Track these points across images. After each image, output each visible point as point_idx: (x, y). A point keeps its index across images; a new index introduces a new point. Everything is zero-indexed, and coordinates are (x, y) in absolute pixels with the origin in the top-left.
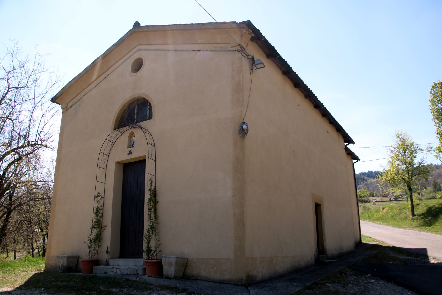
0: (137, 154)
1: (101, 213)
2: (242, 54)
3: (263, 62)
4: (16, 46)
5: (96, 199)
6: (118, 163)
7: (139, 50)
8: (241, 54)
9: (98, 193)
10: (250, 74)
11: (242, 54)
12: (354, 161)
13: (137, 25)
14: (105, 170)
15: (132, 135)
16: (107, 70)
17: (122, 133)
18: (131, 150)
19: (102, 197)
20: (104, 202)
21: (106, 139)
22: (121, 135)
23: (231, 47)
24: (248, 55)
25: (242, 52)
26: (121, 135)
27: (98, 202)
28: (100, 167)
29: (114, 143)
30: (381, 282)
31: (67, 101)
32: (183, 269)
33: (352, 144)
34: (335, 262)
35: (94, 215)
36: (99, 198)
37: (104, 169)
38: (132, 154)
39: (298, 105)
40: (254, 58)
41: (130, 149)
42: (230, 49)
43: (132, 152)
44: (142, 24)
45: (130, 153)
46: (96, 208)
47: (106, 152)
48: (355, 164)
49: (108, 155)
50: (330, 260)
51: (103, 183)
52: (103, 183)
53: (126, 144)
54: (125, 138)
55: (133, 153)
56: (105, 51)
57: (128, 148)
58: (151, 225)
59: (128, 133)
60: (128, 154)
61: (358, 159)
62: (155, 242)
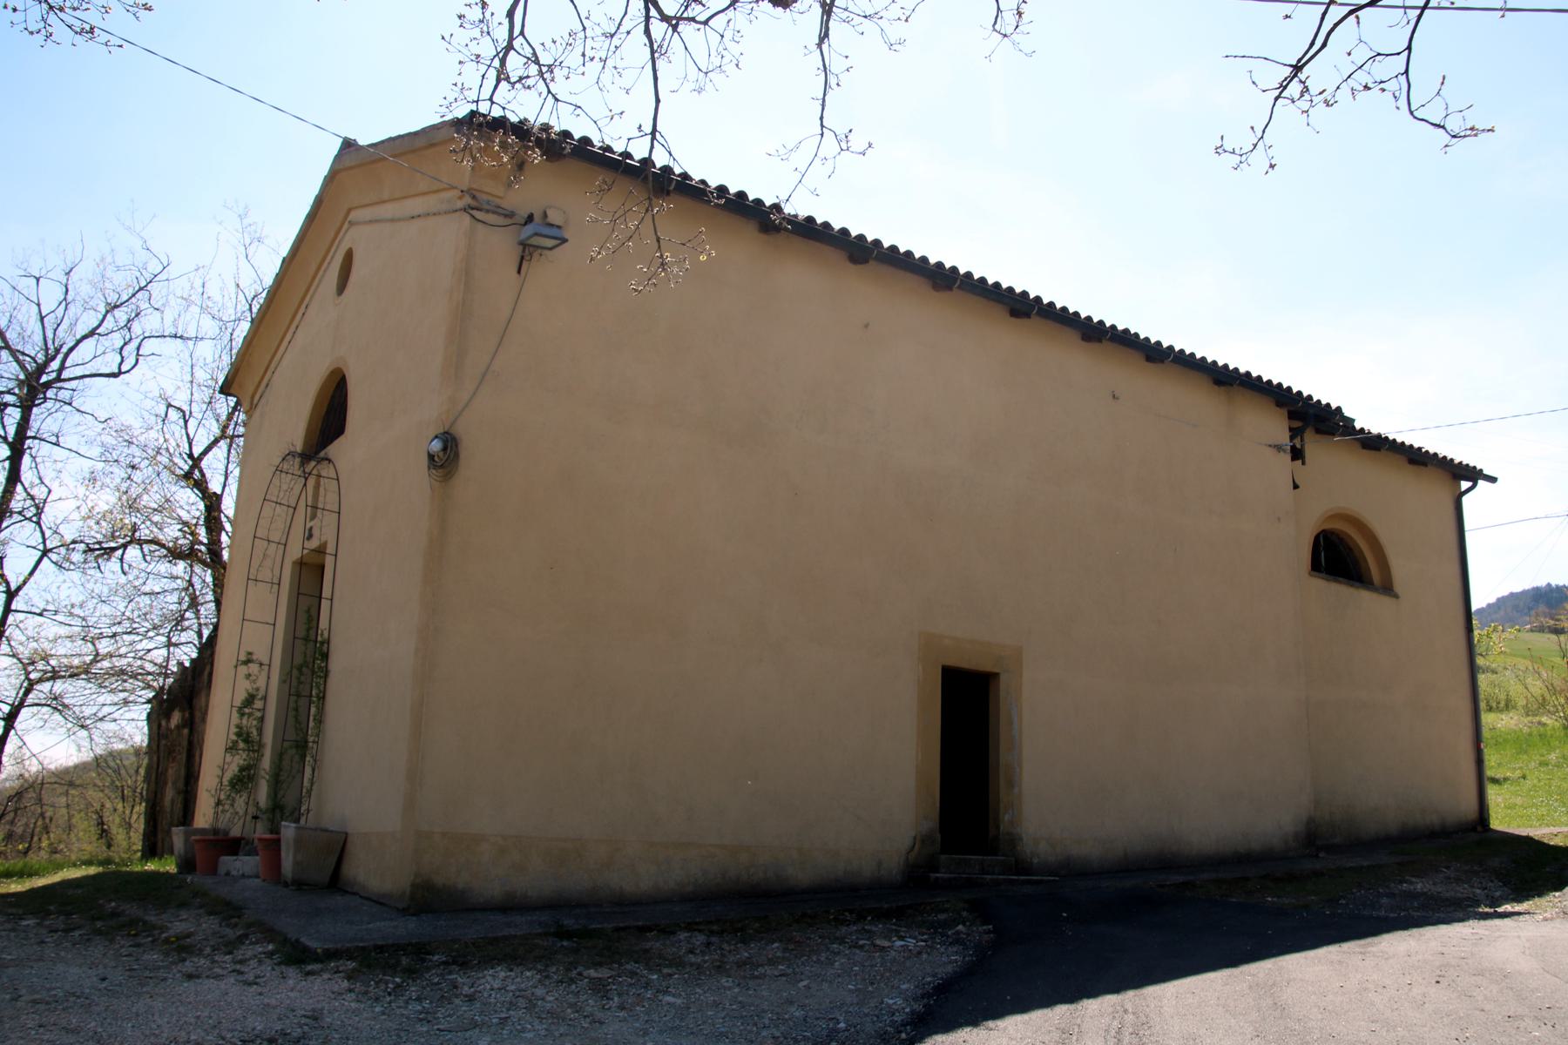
1: (259, 710)
4: (246, 222)
5: (243, 670)
9: (250, 654)
11: (473, 217)
13: (348, 145)
14: (276, 587)
19: (261, 664)
20: (269, 678)
21: (265, 499)
27: (248, 676)
28: (256, 580)
30: (876, 926)
31: (251, 389)
32: (333, 860)
33: (1345, 415)
34: (1049, 881)
35: (235, 715)
36: (254, 668)
37: (272, 583)
44: (363, 141)
46: (248, 694)
48: (1465, 499)
49: (283, 541)
50: (995, 877)
51: (267, 623)
52: (267, 623)
58: (299, 738)
62: (218, 776)
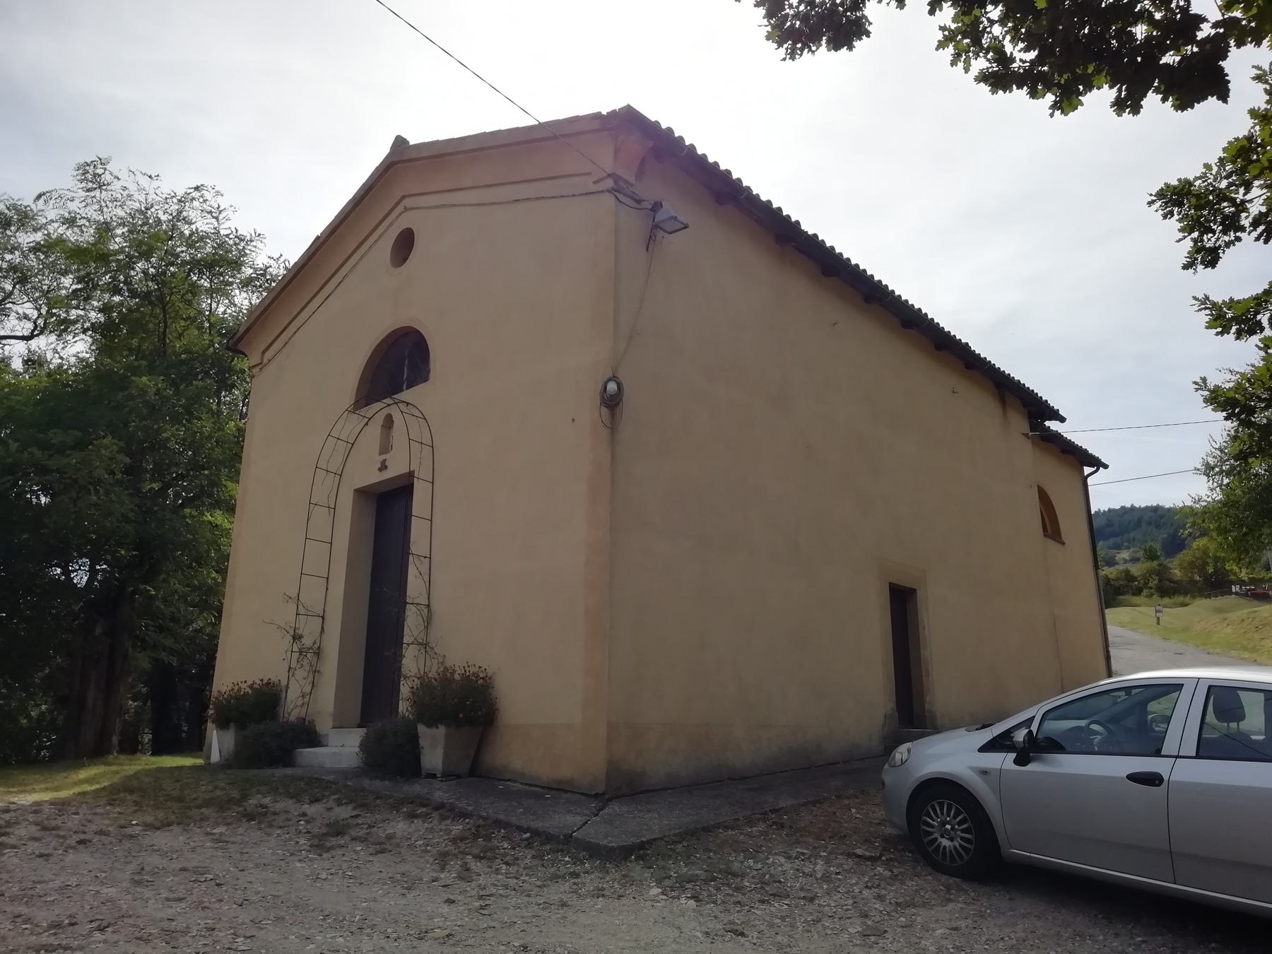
0: (396, 469)
2: (617, 197)
3: (673, 214)
6: (361, 493)
7: (406, 209)
8: (614, 198)
10: (647, 250)
11: (617, 197)
12: (1087, 470)
13: (400, 143)
15: (389, 423)
16: (342, 265)
17: (370, 419)
18: (386, 460)
21: (329, 435)
22: (367, 424)
23: (595, 183)
24: (639, 202)
25: (616, 193)
26: (367, 424)
29: (353, 444)
38: (387, 470)
39: (834, 324)
40: (1186, 185)
41: (383, 457)
42: (594, 188)
43: (387, 463)
45: (383, 467)
47: (335, 466)
53: (376, 446)
54: (375, 430)
55: (389, 468)
56: (333, 218)
57: (381, 454)
59: (380, 418)
60: (380, 470)
61: (1097, 464)
